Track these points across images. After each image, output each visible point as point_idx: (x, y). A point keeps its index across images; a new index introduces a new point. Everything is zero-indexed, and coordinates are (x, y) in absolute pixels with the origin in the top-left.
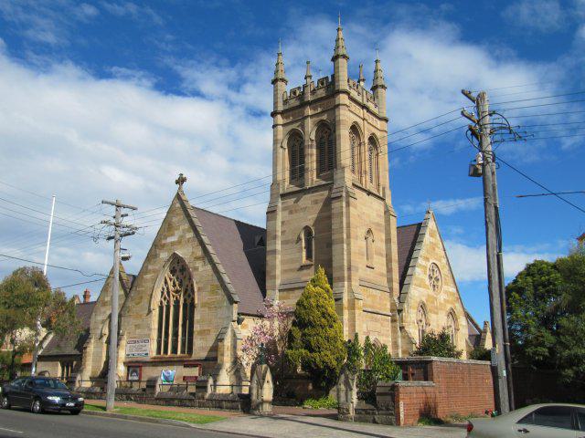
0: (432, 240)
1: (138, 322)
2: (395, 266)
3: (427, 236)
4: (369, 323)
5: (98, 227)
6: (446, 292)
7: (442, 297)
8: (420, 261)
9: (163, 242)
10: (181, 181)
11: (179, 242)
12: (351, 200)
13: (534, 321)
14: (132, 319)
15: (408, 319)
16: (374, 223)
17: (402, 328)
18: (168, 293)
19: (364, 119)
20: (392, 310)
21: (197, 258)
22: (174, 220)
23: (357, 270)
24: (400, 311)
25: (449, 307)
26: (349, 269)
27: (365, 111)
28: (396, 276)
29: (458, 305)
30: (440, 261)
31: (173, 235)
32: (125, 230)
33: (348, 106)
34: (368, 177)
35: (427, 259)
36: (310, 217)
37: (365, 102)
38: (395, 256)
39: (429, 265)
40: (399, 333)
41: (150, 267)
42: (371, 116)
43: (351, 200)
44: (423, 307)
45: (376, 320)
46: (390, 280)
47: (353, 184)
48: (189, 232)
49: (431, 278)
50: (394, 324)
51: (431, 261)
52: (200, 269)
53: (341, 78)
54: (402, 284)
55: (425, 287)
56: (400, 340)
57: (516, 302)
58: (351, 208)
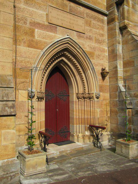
17: (123, 29)
20: (109, 7)
40: (119, 38)
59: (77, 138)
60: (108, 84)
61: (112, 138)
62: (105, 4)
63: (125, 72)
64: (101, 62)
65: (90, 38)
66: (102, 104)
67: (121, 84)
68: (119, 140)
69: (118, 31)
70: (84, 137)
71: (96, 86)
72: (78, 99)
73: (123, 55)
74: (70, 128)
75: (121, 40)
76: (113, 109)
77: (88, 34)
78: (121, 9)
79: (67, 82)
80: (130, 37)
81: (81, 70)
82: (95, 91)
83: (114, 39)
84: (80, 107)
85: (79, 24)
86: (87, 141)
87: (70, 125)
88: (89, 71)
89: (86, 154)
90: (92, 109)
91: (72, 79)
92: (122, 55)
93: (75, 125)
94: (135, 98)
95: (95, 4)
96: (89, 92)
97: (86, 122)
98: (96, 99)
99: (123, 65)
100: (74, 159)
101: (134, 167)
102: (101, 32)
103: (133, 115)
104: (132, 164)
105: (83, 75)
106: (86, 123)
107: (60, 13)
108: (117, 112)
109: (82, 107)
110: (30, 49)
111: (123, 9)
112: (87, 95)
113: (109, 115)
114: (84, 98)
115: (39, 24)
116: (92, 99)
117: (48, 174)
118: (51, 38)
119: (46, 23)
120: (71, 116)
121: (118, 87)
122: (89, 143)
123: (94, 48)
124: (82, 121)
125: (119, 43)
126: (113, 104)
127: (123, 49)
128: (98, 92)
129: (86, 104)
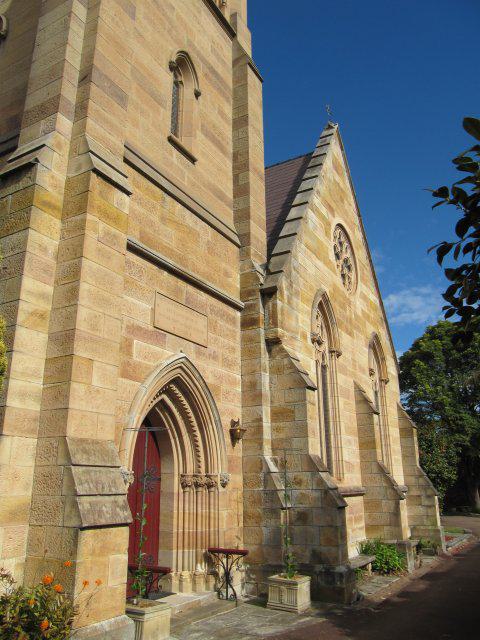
4: (165, 306)
13: (447, 395)
17: (273, 343)
20: (245, 294)
24: (269, 294)
25: (370, 329)
26: (85, 78)
40: (265, 359)
45: (189, 305)
46: (243, 216)
50: (250, 332)
54: (273, 238)
56: (266, 378)
57: (421, 372)
58: (90, 122)
59: (177, 582)
60: (240, 455)
61: (249, 576)
62: (238, 286)
63: (275, 430)
64: (230, 406)
65: (215, 357)
66: (230, 500)
67: (268, 456)
68: (274, 577)
69: (263, 345)
70: (194, 577)
71: (222, 460)
72: (183, 487)
73: (272, 396)
74: (160, 557)
75: (267, 363)
76: (251, 510)
77: (212, 348)
78: (270, 304)
79: (157, 444)
80: (286, 361)
81: (195, 423)
82: (219, 471)
83: (256, 361)
84: (187, 506)
85: (198, 327)
86: (202, 586)
87: (160, 551)
88: (210, 426)
89: (213, 613)
90: (212, 510)
91: (172, 441)
92: (269, 395)
93: (175, 551)
94: (297, 487)
95: (223, 287)
96: (207, 471)
97: (199, 542)
98: (221, 489)
99: (272, 416)
100: (197, 625)
101: (314, 623)
102: (232, 344)
103: (291, 523)
104: (308, 619)
105: (198, 433)
106: (199, 546)
107: (172, 306)
108: (259, 517)
109: (192, 507)
110: (124, 380)
111: (275, 305)
112: (204, 480)
113: (241, 524)
114: (197, 485)
115: (139, 329)
116: (213, 489)
117: (409, 535)
118: (156, 356)
119: (151, 328)
120: (162, 528)
121: (262, 462)
122: (204, 594)
123: (220, 378)
124: (194, 540)
125: (265, 371)
126: (250, 500)
127: (271, 382)
128: (225, 472)
129: (199, 501)
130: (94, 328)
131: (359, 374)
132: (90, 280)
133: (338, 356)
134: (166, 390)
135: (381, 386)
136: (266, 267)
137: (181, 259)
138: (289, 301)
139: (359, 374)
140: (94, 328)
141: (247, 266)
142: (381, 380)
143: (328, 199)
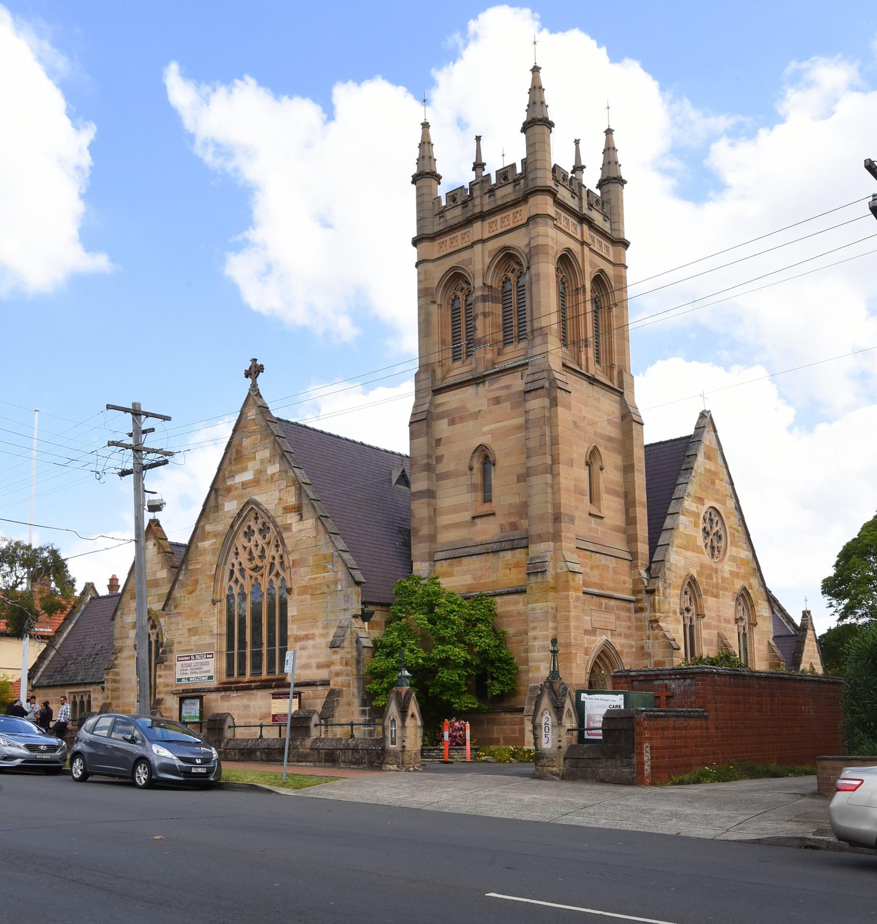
0: (709, 465)
1: (191, 623)
2: (642, 514)
3: (700, 458)
4: (596, 615)
5: (102, 452)
6: (734, 559)
7: (727, 567)
8: (689, 504)
9: (229, 483)
10: (255, 371)
11: (256, 482)
12: (560, 394)
14: (179, 619)
15: (665, 607)
16: (603, 437)
18: (242, 570)
19: (583, 243)
20: (635, 592)
21: (287, 510)
22: (246, 442)
23: (572, 520)
25: (739, 584)
27: (585, 227)
28: (642, 529)
29: (755, 582)
30: (724, 503)
31: (244, 469)
32: (151, 456)
33: (553, 219)
34: (591, 352)
35: (701, 500)
36: (486, 429)
37: (585, 210)
38: (641, 495)
39: (703, 510)
41: (209, 528)
42: (597, 237)
43: (560, 394)
44: (692, 583)
45: (608, 609)
46: (632, 540)
47: (564, 365)
48: (271, 461)
49: (706, 533)
51: (709, 503)
52: (295, 528)
53: (543, 311)
54: (653, 545)
55: (696, 549)
65: (620, 635)
77: (618, 630)
80: (661, 633)
111: (654, 600)
118: (594, 642)
130: (576, 640)
131: (723, 625)
132: (573, 621)
133: (703, 617)
134: (599, 657)
135: (750, 629)
136: (648, 570)
137: (601, 587)
138: (663, 593)
139: (723, 625)
140: (576, 640)
141: (636, 574)
142: (750, 624)
143: (786, 818)
